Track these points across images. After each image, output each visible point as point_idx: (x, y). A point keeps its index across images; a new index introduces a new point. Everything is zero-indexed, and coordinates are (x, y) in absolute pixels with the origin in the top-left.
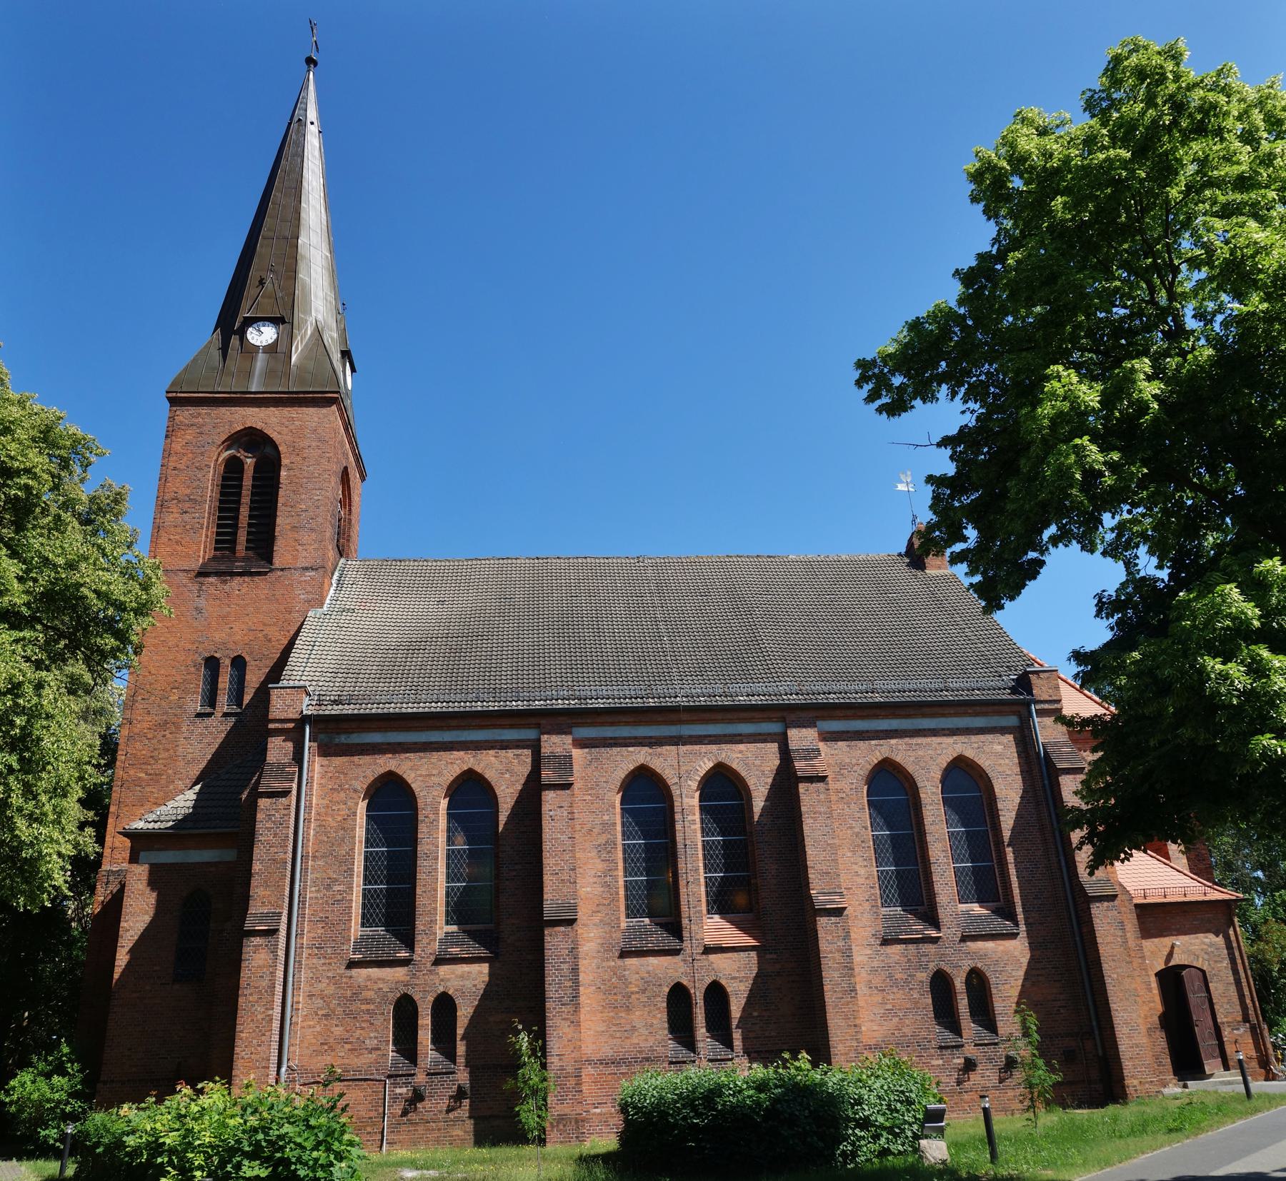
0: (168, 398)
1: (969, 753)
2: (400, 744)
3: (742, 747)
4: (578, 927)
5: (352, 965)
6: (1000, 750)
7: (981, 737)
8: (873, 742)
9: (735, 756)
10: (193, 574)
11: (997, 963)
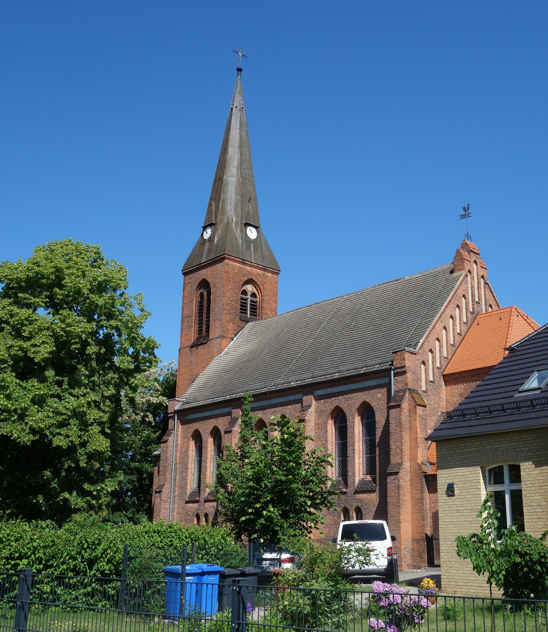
0: (183, 273)
1: (368, 400)
2: (199, 418)
3: (290, 407)
4: (400, 474)
5: (187, 502)
6: (380, 397)
7: (374, 391)
8: (333, 399)
9: (287, 411)
10: (190, 347)
11: (366, 504)
